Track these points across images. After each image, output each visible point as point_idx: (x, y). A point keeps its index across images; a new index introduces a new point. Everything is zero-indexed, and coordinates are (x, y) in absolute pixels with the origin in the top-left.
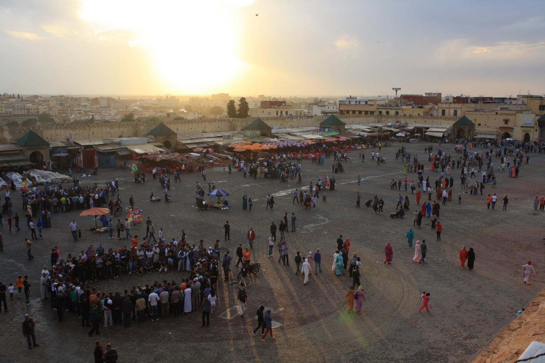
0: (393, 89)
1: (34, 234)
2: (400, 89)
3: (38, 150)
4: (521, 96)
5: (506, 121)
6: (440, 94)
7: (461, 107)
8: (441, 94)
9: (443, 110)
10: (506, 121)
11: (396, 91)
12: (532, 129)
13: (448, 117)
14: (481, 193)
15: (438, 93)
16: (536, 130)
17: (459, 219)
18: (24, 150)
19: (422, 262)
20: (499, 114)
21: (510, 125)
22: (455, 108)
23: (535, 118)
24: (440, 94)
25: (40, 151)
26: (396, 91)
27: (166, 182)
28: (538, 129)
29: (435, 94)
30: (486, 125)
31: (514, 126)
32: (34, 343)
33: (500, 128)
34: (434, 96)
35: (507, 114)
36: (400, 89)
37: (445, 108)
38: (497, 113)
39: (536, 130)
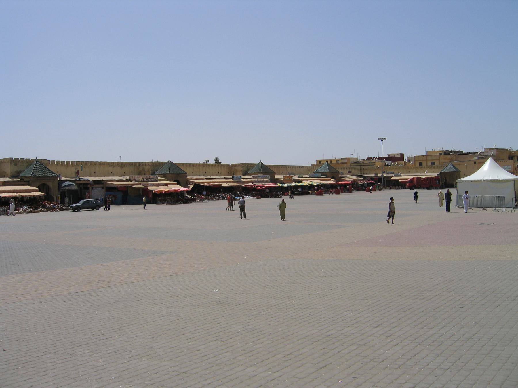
0: (379, 139)
2: (385, 139)
3: (45, 183)
4: (488, 149)
6: (402, 155)
7: (438, 158)
8: (403, 154)
9: (419, 163)
11: (382, 141)
13: (439, 166)
15: (401, 154)
17: (319, 319)
18: (31, 182)
20: (477, 163)
22: (432, 160)
23: (513, 164)
24: (402, 155)
25: (47, 183)
26: (382, 141)
27: (238, 198)
30: (465, 174)
34: (398, 156)
36: (385, 139)
38: (475, 163)
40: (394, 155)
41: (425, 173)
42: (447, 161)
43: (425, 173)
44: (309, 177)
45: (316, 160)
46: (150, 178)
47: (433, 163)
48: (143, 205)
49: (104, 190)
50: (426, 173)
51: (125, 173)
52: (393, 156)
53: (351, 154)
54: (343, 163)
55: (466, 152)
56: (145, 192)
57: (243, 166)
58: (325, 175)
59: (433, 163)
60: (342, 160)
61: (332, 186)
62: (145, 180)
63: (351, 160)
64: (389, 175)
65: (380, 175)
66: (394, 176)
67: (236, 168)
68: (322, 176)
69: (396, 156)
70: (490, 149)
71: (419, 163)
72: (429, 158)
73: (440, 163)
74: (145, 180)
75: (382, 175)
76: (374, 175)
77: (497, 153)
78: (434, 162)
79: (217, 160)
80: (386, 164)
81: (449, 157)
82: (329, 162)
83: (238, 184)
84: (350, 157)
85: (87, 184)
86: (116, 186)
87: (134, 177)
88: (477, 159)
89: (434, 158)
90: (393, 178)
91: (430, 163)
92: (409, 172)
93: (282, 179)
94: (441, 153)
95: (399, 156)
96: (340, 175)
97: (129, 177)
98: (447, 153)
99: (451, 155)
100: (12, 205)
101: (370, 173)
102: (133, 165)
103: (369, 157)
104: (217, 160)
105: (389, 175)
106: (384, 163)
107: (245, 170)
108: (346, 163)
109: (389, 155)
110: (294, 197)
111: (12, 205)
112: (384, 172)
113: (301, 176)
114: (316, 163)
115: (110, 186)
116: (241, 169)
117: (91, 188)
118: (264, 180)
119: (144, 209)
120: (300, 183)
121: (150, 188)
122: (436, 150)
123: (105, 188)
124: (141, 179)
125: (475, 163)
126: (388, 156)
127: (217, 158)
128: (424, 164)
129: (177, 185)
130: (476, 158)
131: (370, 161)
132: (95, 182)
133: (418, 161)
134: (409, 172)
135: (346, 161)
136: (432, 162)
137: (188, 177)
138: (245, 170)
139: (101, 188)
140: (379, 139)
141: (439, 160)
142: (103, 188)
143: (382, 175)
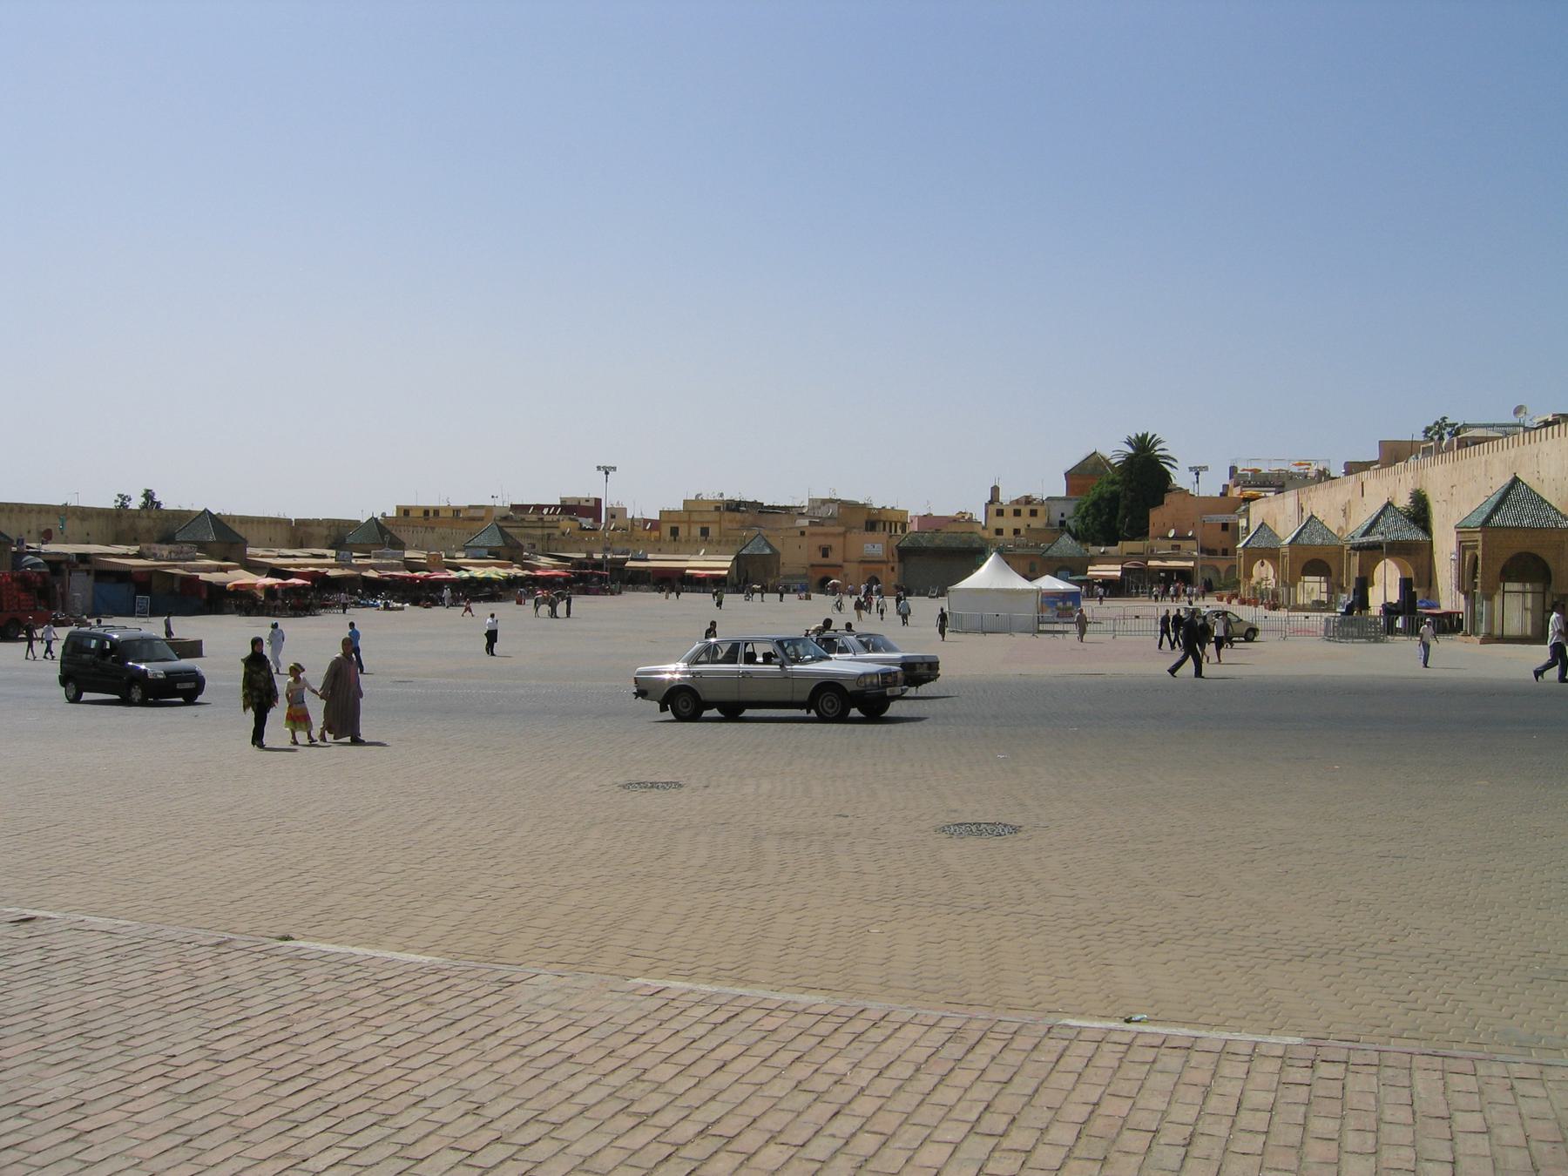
0: (599, 468)
1: (748, 713)
5: (825, 552)
6: (598, 501)
10: (825, 552)
11: (607, 473)
12: (884, 567)
14: (1217, 660)
15: (596, 499)
16: (893, 569)
19: (48, 655)
21: (834, 558)
23: (887, 542)
24: (598, 501)
26: (607, 473)
28: (896, 566)
29: (587, 501)
31: (844, 561)
32: (1545, 953)
33: (812, 566)
35: (826, 535)
37: (680, 522)
38: (803, 533)
39: (893, 569)
40: (579, 500)
41: (701, 554)
42: (735, 526)
43: (701, 554)
44: (465, 558)
45: (397, 507)
46: (181, 552)
47: (705, 532)
48: (779, 595)
49: (92, 578)
50: (704, 554)
51: (88, 534)
52: (575, 503)
53: (493, 497)
54: (473, 519)
55: (781, 505)
56: (191, 583)
57: (330, 526)
58: (495, 553)
59: (705, 532)
60: (472, 511)
61: (512, 583)
62: (173, 555)
63: (496, 513)
64: (617, 557)
65: (598, 556)
66: (632, 559)
67: (310, 530)
68: (489, 554)
69: (583, 503)
70: (824, 502)
71: (672, 528)
72: (695, 517)
73: (720, 531)
74: (173, 555)
75: (605, 557)
76: (584, 555)
77: (841, 510)
78: (708, 529)
79: (148, 495)
80: (581, 524)
81: (738, 516)
82: (431, 514)
83: (355, 573)
84: (489, 502)
85: (60, 562)
86: (133, 570)
87: (154, 548)
88: (807, 524)
89: (708, 517)
90: (629, 564)
91: (696, 531)
92: (660, 550)
93: (354, 554)
94: (720, 507)
95: (592, 504)
96: (525, 554)
97: (138, 548)
98: (734, 507)
99: (743, 511)
100: (447, 593)
101: (564, 548)
102: (265, 523)
103: (525, 503)
104: (148, 495)
105: (617, 557)
106: (577, 524)
107: (333, 534)
108: (481, 519)
109: (563, 500)
110: (813, 595)
111: (447, 593)
112: (607, 550)
113: (451, 555)
114: (395, 515)
115: (106, 568)
116: (326, 532)
117: (67, 573)
118: (394, 561)
119: (781, 600)
120: (457, 571)
121: (203, 576)
122: (704, 498)
123: (93, 572)
124: (165, 553)
125: (803, 533)
126: (561, 502)
127: (148, 491)
128: (683, 532)
129: (242, 571)
130: (805, 522)
131: (541, 516)
132: (83, 558)
133: (668, 522)
134: (660, 550)
135: (482, 513)
136: (702, 528)
137: (249, 551)
138: (333, 534)
139: (85, 574)
140: (599, 468)
141: (720, 522)
142: (88, 572)
143: (605, 557)
